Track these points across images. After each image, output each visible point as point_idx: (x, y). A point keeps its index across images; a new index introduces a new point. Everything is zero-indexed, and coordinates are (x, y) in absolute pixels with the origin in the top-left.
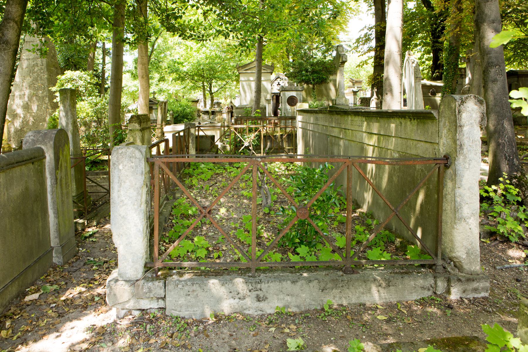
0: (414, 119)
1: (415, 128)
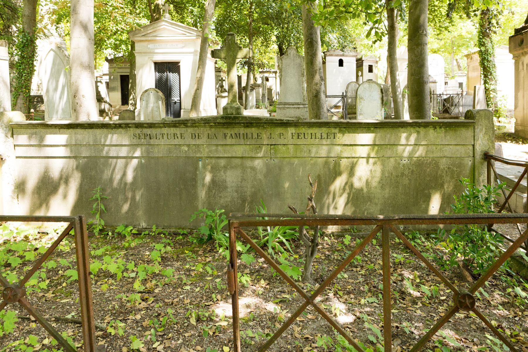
0: (441, 128)
1: (442, 135)
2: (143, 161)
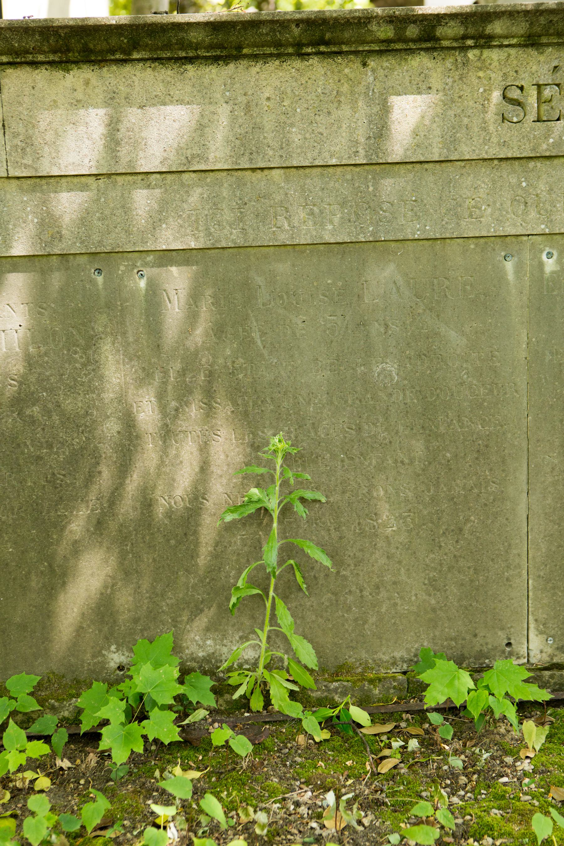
2: (550, 265)
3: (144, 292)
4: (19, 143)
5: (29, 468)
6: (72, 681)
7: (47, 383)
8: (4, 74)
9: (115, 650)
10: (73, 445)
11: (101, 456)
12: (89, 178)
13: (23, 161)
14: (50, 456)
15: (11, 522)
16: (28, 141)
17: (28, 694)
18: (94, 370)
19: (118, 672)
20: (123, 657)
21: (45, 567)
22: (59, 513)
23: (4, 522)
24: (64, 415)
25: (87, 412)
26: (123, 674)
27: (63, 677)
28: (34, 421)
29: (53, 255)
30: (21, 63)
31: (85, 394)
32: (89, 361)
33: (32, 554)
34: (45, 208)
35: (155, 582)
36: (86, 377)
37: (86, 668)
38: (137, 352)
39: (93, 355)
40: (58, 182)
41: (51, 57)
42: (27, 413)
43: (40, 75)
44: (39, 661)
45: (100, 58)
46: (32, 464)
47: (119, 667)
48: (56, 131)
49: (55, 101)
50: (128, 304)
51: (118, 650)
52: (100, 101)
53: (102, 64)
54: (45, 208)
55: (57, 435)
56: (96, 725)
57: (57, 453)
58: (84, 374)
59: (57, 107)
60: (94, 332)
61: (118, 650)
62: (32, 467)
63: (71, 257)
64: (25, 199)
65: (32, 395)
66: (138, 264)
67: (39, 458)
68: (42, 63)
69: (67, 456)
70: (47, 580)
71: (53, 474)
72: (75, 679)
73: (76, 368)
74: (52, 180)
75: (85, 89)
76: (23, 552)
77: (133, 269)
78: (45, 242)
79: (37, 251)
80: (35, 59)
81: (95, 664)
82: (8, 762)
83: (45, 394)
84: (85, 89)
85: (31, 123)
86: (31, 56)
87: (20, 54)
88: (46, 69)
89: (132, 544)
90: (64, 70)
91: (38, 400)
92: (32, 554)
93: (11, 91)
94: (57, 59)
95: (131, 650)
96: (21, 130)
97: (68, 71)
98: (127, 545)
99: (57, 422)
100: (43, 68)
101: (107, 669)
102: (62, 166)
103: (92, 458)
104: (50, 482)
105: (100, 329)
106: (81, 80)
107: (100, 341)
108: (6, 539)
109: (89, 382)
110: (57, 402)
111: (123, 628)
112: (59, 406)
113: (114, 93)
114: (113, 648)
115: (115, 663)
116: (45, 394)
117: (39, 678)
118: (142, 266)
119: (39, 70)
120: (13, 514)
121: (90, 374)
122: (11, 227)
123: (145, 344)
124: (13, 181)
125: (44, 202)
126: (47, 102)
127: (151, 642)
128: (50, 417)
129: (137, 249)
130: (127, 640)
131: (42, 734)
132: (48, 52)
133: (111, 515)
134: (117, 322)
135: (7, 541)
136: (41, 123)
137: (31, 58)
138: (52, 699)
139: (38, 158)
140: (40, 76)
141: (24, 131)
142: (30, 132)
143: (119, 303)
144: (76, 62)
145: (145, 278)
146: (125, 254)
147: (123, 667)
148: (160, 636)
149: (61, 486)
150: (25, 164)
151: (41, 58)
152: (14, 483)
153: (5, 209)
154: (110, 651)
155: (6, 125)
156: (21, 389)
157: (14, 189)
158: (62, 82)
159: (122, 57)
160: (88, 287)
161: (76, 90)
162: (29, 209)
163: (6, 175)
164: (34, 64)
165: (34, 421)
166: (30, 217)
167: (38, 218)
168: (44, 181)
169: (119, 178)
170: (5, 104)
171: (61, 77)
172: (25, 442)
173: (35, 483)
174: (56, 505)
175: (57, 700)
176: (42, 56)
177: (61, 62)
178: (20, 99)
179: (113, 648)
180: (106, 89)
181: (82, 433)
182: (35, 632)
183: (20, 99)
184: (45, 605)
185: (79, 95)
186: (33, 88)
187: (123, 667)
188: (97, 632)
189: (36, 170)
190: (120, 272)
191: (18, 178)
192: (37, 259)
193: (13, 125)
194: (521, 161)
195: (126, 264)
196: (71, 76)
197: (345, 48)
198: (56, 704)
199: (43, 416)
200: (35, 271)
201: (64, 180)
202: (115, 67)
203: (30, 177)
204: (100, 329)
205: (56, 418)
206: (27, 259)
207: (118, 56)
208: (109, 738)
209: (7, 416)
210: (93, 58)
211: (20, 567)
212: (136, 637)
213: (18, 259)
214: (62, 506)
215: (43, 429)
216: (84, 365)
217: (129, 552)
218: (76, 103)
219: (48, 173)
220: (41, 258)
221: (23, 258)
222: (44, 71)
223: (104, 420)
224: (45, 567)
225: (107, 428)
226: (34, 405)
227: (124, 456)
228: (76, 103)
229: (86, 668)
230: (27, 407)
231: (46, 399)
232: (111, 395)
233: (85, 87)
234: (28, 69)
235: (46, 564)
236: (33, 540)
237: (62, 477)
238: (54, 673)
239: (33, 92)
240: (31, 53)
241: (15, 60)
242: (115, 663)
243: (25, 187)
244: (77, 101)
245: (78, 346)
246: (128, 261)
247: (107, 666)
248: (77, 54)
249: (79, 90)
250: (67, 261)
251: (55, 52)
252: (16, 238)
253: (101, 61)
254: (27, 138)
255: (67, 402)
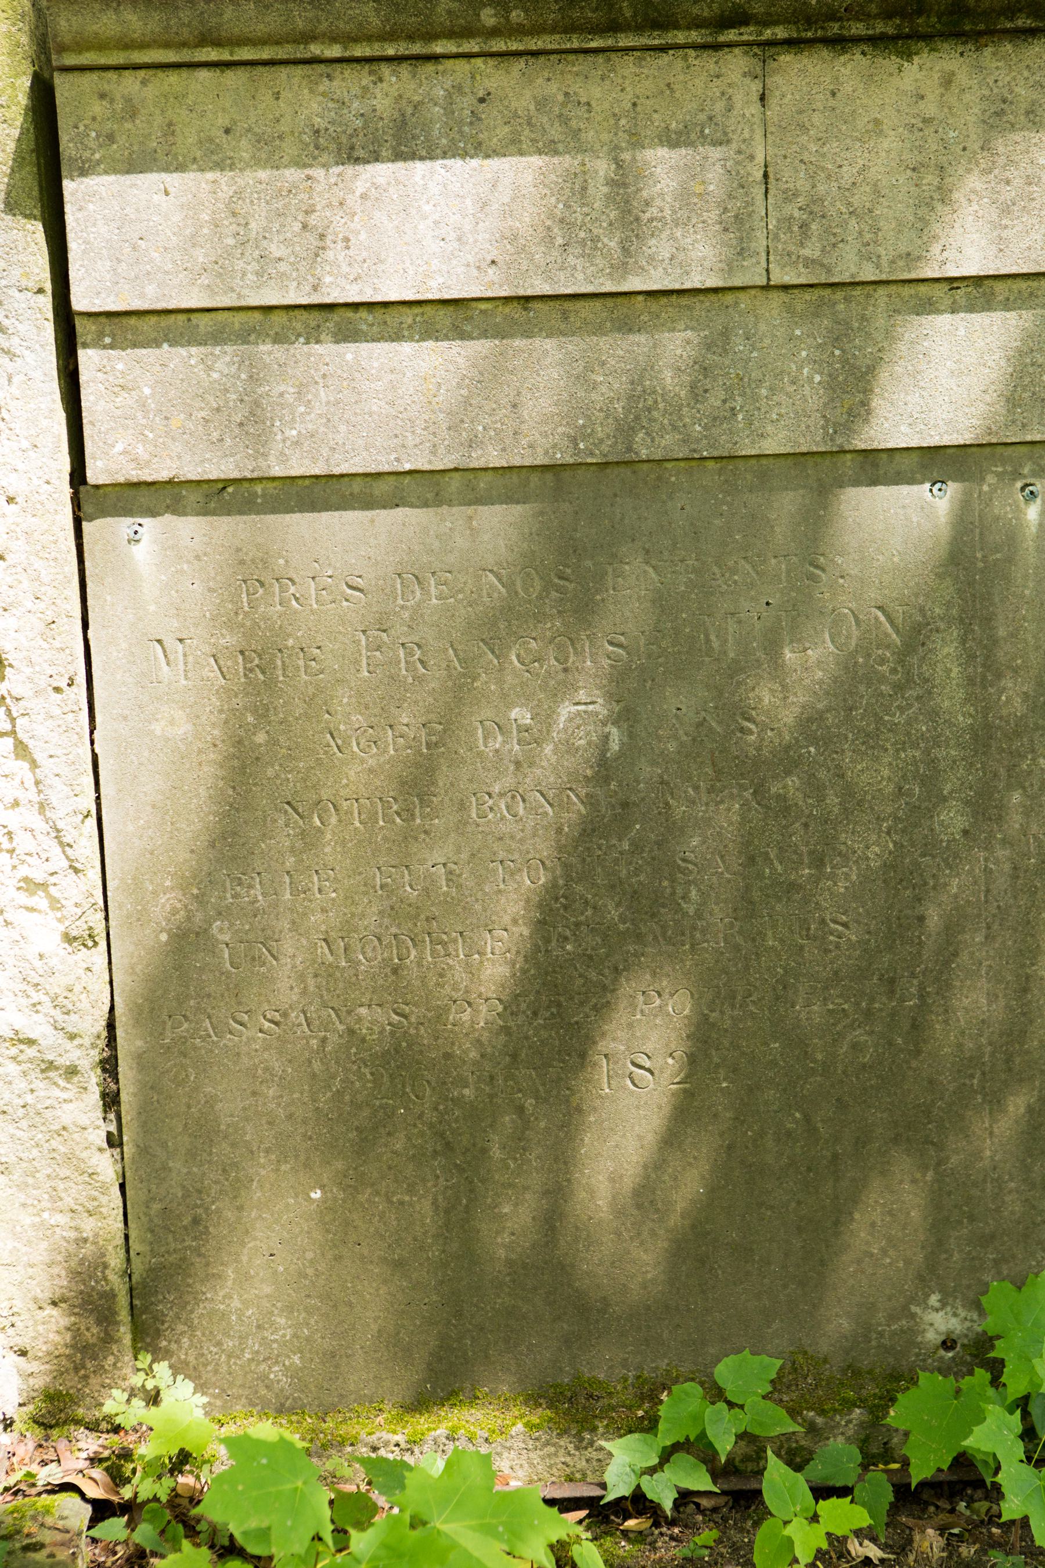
3: (1034, 530)
4: (797, 214)
5: (773, 908)
6: (844, 1371)
7: (819, 727)
8: (775, 65)
9: (937, 1305)
10: (868, 859)
11: (926, 884)
12: (937, 285)
13: (802, 252)
14: (817, 882)
15: (728, 1024)
16: (816, 208)
17: (764, 1397)
18: (919, 698)
19: (942, 1352)
20: (954, 1320)
21: (796, 1121)
22: (831, 1007)
23: (713, 1025)
24: (852, 795)
25: (900, 789)
26: (953, 1358)
27: (825, 1361)
28: (787, 809)
29: (850, 451)
30: (811, 42)
31: (897, 750)
32: (909, 681)
33: (771, 1094)
34: (837, 352)
35: (1031, 1156)
36: (902, 713)
37: (874, 1343)
38: (1014, 659)
39: (920, 667)
40: (868, 296)
41: (880, 27)
42: (773, 790)
43: (849, 66)
44: (775, 1326)
45: (982, 27)
46: (779, 899)
47: (944, 1343)
48: (875, 185)
49: (877, 122)
50: (998, 556)
51: (944, 1304)
52: (973, 119)
53: (983, 41)
54: (837, 352)
55: (835, 838)
56: (945, 1467)
57: (832, 877)
58: (899, 707)
59: (881, 133)
60: (924, 616)
61: (944, 1304)
62: (778, 907)
63: (884, 456)
64: (798, 332)
65: (786, 752)
66: (1026, 471)
67: (793, 887)
68: (857, 40)
69: (853, 884)
70: (798, 1150)
71: (823, 921)
72: (849, 1367)
73: (881, 695)
74: (857, 292)
75: (942, 95)
76: (751, 1090)
77: (1014, 480)
78: (834, 424)
79: (817, 444)
80: (845, 32)
81: (894, 1333)
82: (790, 1542)
83: (812, 749)
84: (942, 95)
85: (823, 169)
86: (837, 25)
87: (816, 22)
88: (864, 53)
89: (983, 1074)
90: (900, 54)
91: (796, 763)
92: (771, 1094)
93: (786, 101)
94: (891, 31)
95: (978, 1306)
96: (802, 184)
97: (908, 56)
98: (972, 1076)
99: (836, 810)
100: (857, 51)
101: (919, 1345)
102: (884, 262)
103: (906, 888)
104: (815, 938)
105: (937, 610)
106: (936, 76)
107: (935, 636)
108: (716, 1060)
109: (909, 723)
110: (838, 767)
111: (956, 1256)
112: (842, 776)
113: (1004, 101)
114: (934, 1299)
115: (937, 1332)
116: (812, 749)
117: (779, 1363)
118: (1034, 474)
119: (847, 56)
120: (733, 1007)
121: (911, 706)
122: (764, 392)
123: (1031, 641)
124: (774, 295)
125: (837, 339)
126: (861, 123)
127: (1020, 1288)
128: (821, 799)
129: (1029, 438)
130: (965, 1282)
131: (831, 1483)
132: (876, 16)
133: (941, 1010)
134: (974, 595)
135: (718, 1066)
136: (845, 169)
137: (836, 31)
138: (808, 1409)
139: (834, 245)
140: (849, 70)
141: (808, 187)
142: (821, 188)
143: (979, 555)
144: (927, 38)
145: (1039, 501)
146: (1000, 450)
147: (954, 1342)
148: (1037, 1275)
149: (838, 946)
150: (806, 258)
151: (857, 28)
152: (739, 940)
153: (755, 354)
154: (927, 1307)
155: (771, 175)
156: (763, 739)
157: (775, 312)
158: (896, 81)
159: (1029, 23)
160: (915, 519)
161: (922, 97)
162: (804, 354)
163: (764, 282)
164: (840, 43)
165: (787, 809)
166: (805, 371)
167: (821, 374)
168: (839, 295)
169: (999, 286)
170: (771, 129)
171: (894, 68)
172: (767, 853)
173: (782, 941)
174: (826, 988)
175: (822, 1412)
176: (860, 25)
177: (895, 38)
178: (804, 118)
179: (934, 1299)
180: (987, 93)
181: (888, 833)
182: (769, 1263)
183: (804, 118)
184: (793, 1205)
185: (930, 108)
186: (833, 94)
187: (954, 1342)
188: (901, 1264)
189: (829, 271)
190: (985, 488)
191: (786, 288)
192: (810, 461)
193: (786, 174)
194: (291, 313)
195: (1000, 469)
196: (916, 67)
197: (681, 37)
198: (820, 1420)
199: (806, 796)
200: (805, 487)
201: (882, 291)
202: (1009, 47)
203: (811, 286)
204: (937, 610)
205: (832, 800)
206: (790, 461)
207: (1022, 22)
208: (1016, 1496)
209: (732, 796)
210: (967, 28)
211: (743, 1122)
212: (987, 1278)
213: (771, 460)
214: (838, 991)
215: (806, 825)
216: (899, 688)
217: (976, 1092)
218: (921, 125)
219: (852, 276)
220: (819, 459)
221: (782, 459)
222: (858, 56)
223: (935, 806)
224: (796, 1121)
225: (941, 823)
226: (788, 773)
227: (975, 883)
228: (921, 125)
229: (874, 1343)
230: (775, 777)
231: (815, 762)
232: (953, 753)
233: (942, 90)
234: (825, 53)
235: (798, 1115)
236: (773, 1063)
237: (840, 928)
238: (805, 1353)
239: (832, 102)
240: (840, 19)
241: (803, 34)
242: (937, 1332)
243: (799, 307)
244: (925, 121)
245: (888, 647)
246: (1003, 465)
247: (919, 1339)
248: (934, 19)
249: (930, 97)
250: (875, 466)
251: (888, 15)
252: (774, 416)
253: (980, 34)
254: (814, 202)
255: (859, 767)
